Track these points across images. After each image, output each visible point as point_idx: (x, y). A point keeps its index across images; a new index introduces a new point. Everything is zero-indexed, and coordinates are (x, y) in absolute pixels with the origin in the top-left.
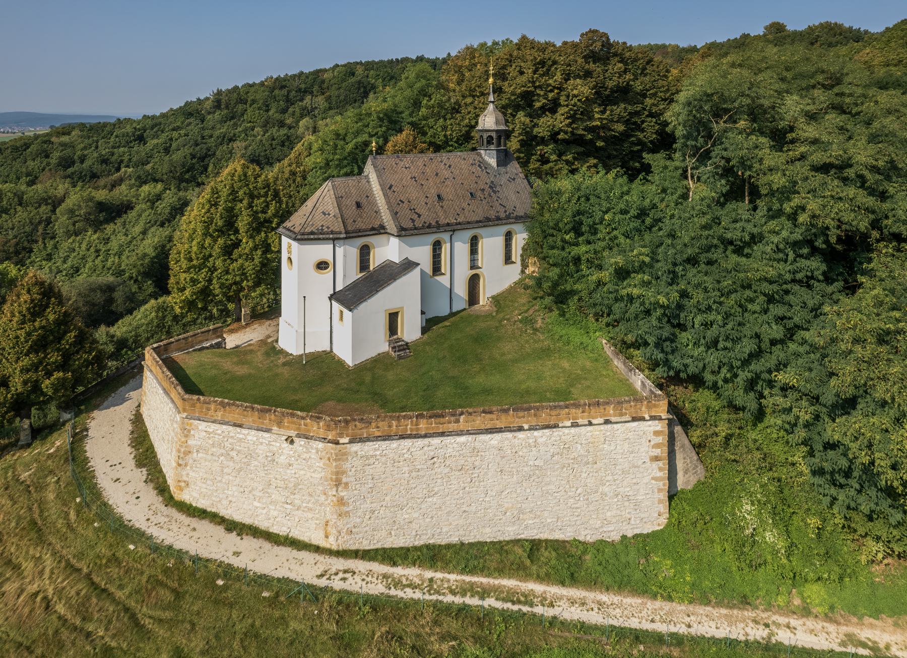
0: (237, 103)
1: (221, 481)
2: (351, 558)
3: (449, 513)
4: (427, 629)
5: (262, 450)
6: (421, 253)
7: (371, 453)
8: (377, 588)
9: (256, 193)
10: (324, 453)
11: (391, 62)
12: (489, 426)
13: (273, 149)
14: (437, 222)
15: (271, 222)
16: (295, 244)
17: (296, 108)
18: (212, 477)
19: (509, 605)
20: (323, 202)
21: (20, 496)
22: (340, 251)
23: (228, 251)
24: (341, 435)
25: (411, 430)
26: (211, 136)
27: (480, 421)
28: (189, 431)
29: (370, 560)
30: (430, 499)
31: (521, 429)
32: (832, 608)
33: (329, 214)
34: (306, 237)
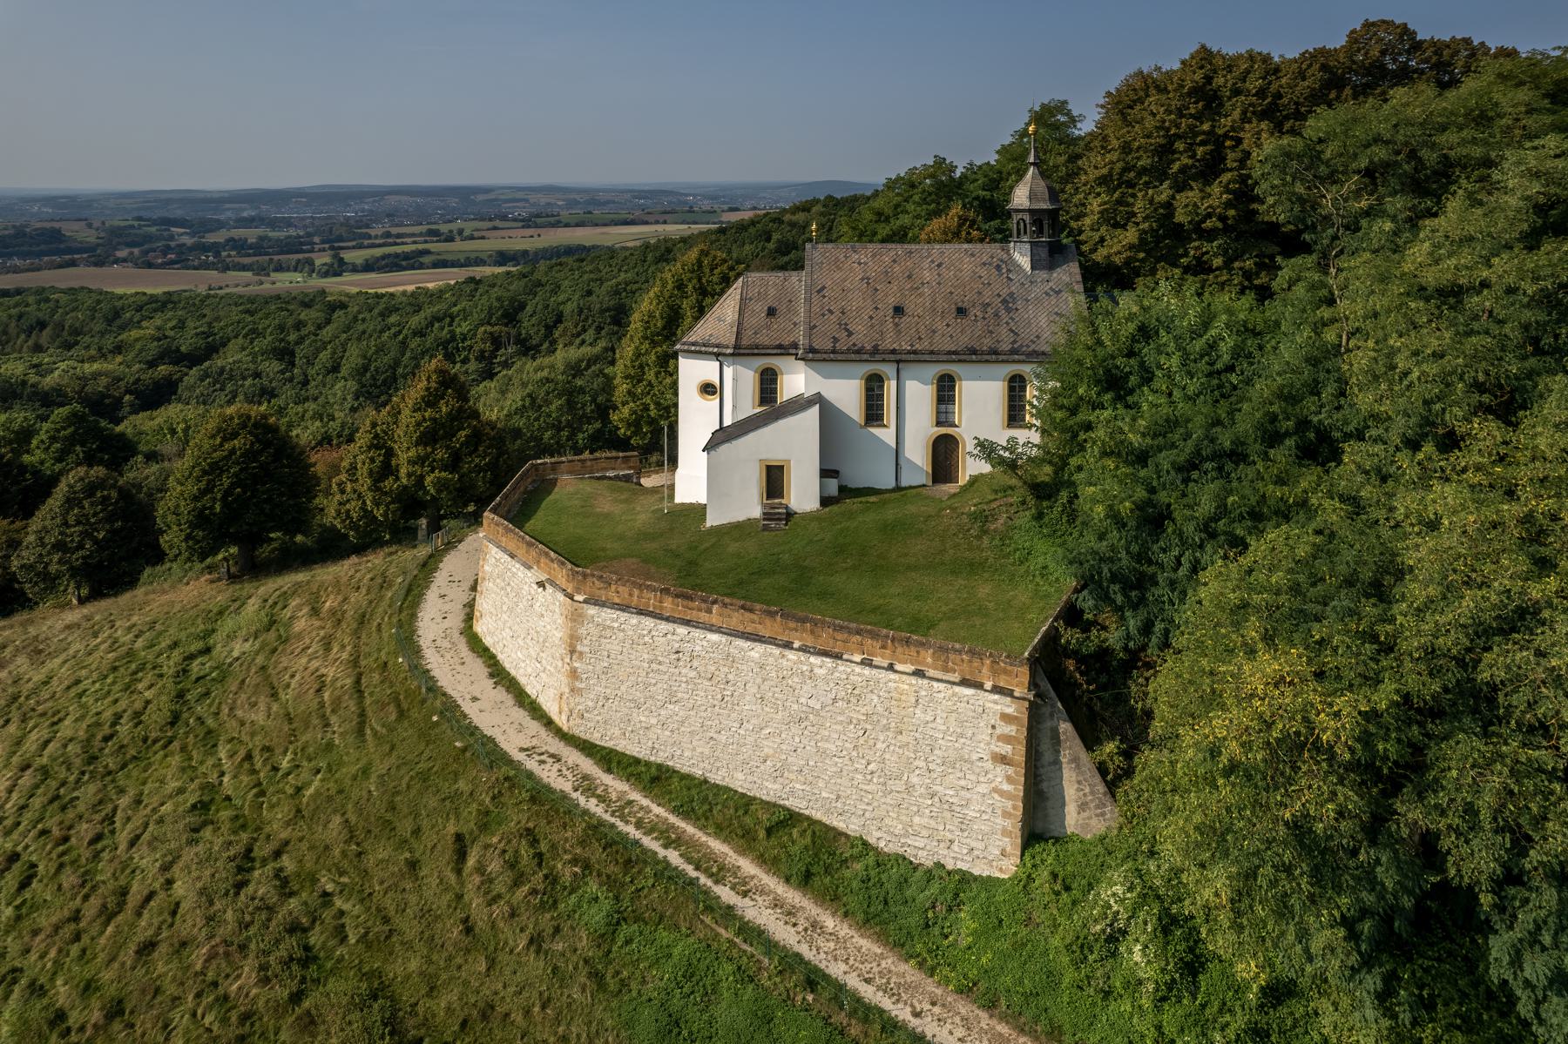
6: (846, 392)
12: (749, 630)
24: (578, 591)
27: (736, 619)
31: (788, 645)
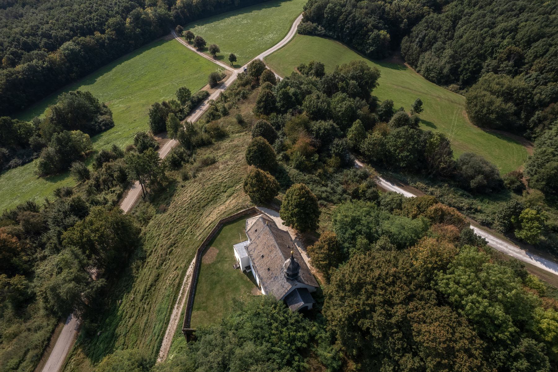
20: (432, 212)
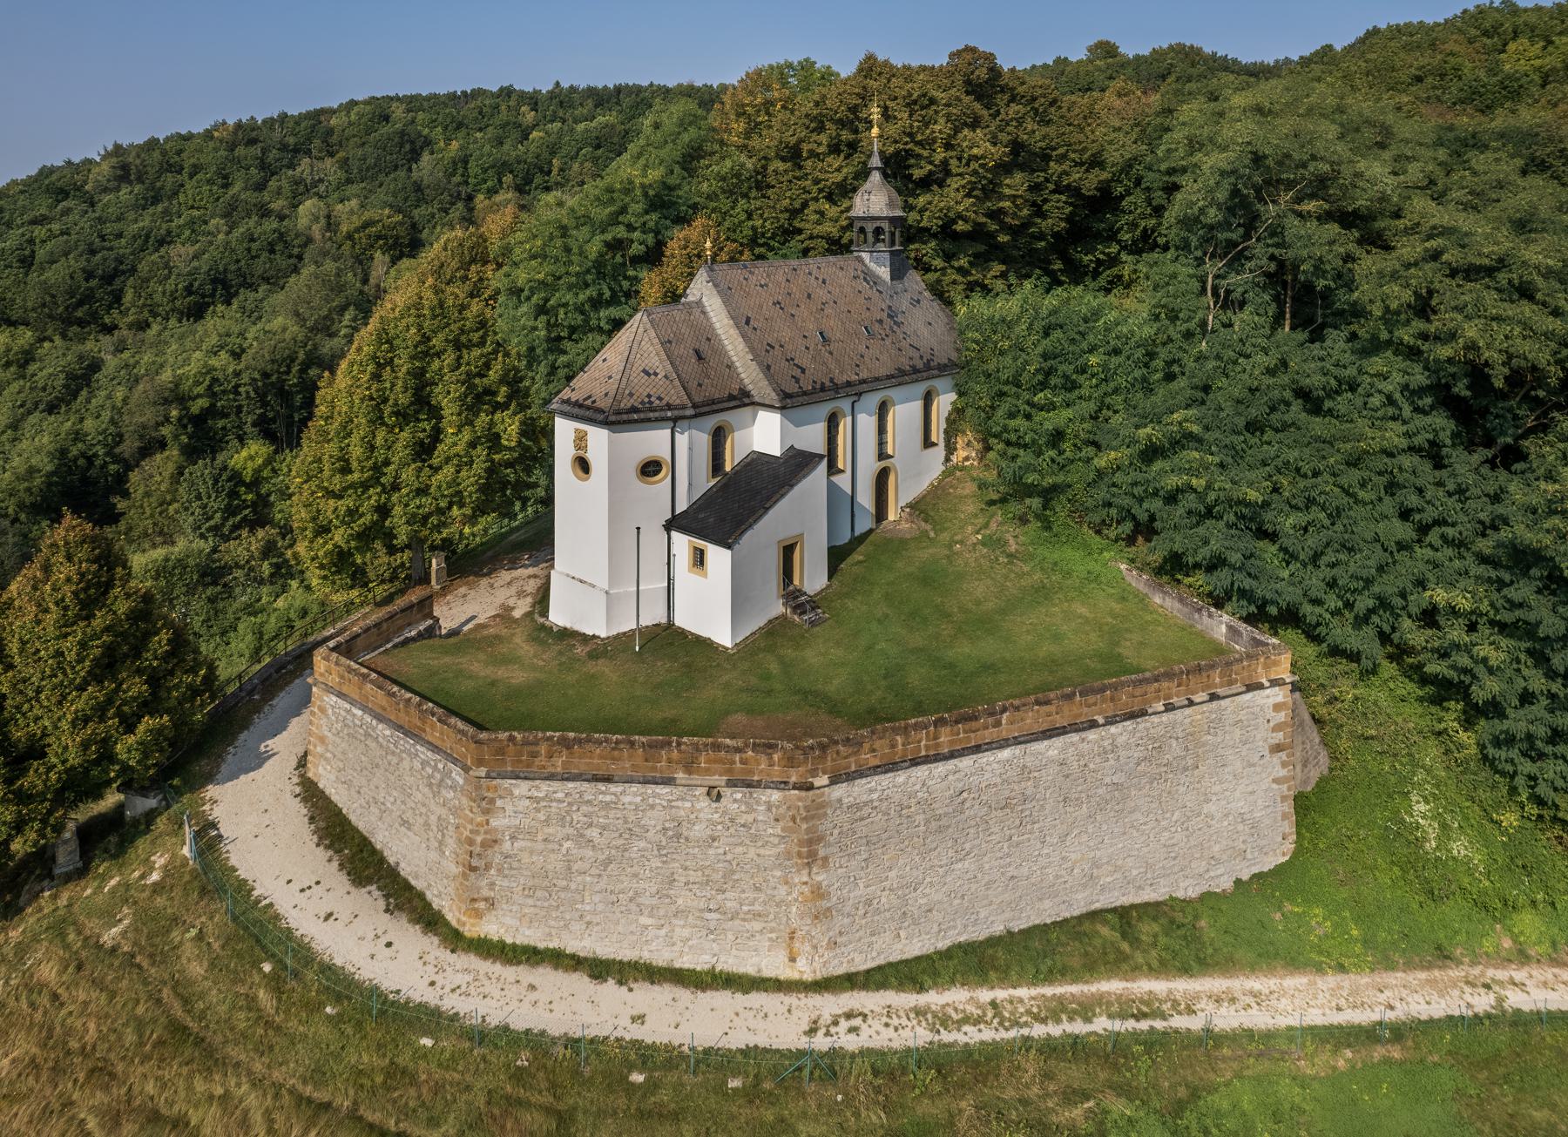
0: (160, 173)
1: (566, 889)
2: (843, 990)
3: (988, 885)
4: (1036, 1090)
5: (653, 819)
7: (865, 798)
8: (918, 1036)
9: (463, 339)
10: (782, 810)
11: (452, 96)
12: (1045, 727)
13: (253, 258)
14: (832, 380)
15: (494, 394)
16: (598, 438)
17: (282, 181)
18: (546, 883)
19: (1131, 1024)
21: (118, 979)
22: (682, 440)
23: (423, 451)
24: (814, 772)
25: (927, 748)
26: (120, 235)
27: (1033, 718)
28: (492, 801)
29: (878, 989)
30: (960, 865)
31: (1093, 725)
32: (1554, 944)
33: (656, 374)
34: (625, 417)
